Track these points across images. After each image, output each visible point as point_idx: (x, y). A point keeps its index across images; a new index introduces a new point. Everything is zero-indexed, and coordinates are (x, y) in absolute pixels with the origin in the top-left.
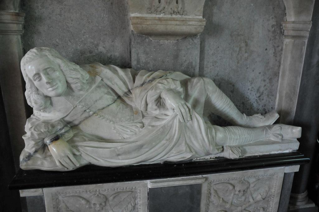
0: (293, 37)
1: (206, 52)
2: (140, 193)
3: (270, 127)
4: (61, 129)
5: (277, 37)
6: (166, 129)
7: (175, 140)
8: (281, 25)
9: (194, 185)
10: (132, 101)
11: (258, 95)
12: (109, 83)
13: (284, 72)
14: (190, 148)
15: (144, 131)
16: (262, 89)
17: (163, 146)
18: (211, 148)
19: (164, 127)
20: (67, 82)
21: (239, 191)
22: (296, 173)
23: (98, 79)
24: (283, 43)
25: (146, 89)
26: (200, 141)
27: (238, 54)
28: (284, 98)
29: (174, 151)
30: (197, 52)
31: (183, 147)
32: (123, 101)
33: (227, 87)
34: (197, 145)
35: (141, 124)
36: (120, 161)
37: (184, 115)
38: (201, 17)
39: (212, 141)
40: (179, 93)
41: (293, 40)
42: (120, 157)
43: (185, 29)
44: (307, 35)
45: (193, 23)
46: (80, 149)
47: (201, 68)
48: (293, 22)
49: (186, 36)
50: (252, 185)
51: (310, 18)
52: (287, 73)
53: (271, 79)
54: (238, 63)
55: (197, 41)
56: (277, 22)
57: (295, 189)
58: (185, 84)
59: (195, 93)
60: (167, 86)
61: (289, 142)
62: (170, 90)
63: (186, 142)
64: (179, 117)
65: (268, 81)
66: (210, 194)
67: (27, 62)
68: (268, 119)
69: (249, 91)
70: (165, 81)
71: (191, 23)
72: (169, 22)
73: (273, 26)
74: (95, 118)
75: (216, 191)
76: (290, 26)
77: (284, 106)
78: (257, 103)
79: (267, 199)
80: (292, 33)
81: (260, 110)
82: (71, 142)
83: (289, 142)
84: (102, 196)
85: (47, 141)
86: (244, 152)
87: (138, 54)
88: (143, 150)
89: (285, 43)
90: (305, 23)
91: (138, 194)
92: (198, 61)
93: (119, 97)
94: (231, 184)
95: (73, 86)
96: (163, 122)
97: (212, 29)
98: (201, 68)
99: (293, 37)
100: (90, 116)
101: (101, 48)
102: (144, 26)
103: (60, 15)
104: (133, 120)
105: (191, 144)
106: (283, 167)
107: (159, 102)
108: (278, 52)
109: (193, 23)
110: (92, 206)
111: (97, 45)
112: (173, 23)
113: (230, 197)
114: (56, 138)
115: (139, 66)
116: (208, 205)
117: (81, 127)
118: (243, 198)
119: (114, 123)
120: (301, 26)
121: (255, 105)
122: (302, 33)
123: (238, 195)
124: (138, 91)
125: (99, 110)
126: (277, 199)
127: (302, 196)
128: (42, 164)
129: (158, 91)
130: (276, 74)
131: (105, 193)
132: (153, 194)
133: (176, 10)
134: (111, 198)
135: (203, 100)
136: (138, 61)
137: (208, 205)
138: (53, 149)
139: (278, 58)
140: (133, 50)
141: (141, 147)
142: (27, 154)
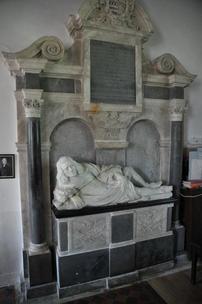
0: (165, 147)
1: (127, 156)
2: (108, 219)
3: (159, 187)
4: (75, 191)
5: (158, 147)
6: (118, 188)
7: (122, 193)
8: (159, 142)
9: (131, 214)
10: (101, 178)
11: (151, 174)
12: (91, 171)
13: (162, 163)
14: (128, 196)
15: (109, 190)
16: (153, 171)
17: (117, 196)
18: (137, 196)
19: (117, 188)
20: (77, 171)
21: (149, 217)
22: (172, 207)
23: (87, 169)
24: (160, 150)
25: (108, 173)
26: (131, 194)
27: (141, 156)
28: (163, 175)
29: (122, 198)
30: (124, 156)
31: (126, 196)
32: (97, 179)
33: (139, 171)
34: (131, 195)
35: (106, 188)
36: (101, 203)
37: (125, 182)
38: (126, 141)
39: (137, 192)
40: (121, 173)
41: (164, 148)
42: (101, 201)
43: (120, 146)
44: (170, 146)
45: (124, 144)
46: (84, 199)
47: (126, 163)
48: (164, 141)
49: (119, 149)
50: (154, 214)
51: (171, 139)
52: (164, 163)
53: (156, 167)
54: (141, 160)
55: (124, 151)
56: (157, 140)
57: (173, 220)
58: (122, 170)
59: (127, 173)
60: (116, 171)
61: (168, 193)
62: (118, 172)
63: (127, 194)
64: (123, 183)
65: (155, 167)
66: (137, 219)
67: (63, 163)
68: (158, 184)
69: (147, 173)
70: (115, 169)
71: (123, 144)
72: (114, 144)
73: (155, 142)
74: (88, 186)
75: (139, 218)
76: (163, 142)
77: (164, 178)
78: (151, 178)
79: (161, 221)
80: (164, 145)
81: (177, 107)
82: (79, 196)
83: (168, 193)
84: (92, 222)
85: (70, 196)
86: (150, 198)
87: (99, 158)
88: (110, 198)
89: (161, 149)
90: (168, 141)
91: (107, 220)
92: (125, 160)
93: (95, 177)
94: (146, 214)
95: (79, 172)
96: (116, 186)
97: (131, 145)
98: (126, 163)
99: (165, 147)
100: (86, 185)
101: (82, 156)
102: (104, 146)
103: (66, 142)
104: (103, 186)
105: (128, 195)
106: (167, 205)
107: (114, 178)
108: (158, 154)
109: (124, 144)
110: (87, 226)
111: (81, 155)
112: (116, 144)
113: (145, 220)
114: (74, 195)
115: (99, 163)
116: (136, 225)
117: (82, 190)
118: (151, 220)
119: (95, 188)
120: (167, 142)
121: (150, 179)
122: (168, 145)
123: (149, 219)
124: (104, 174)
125: (89, 182)
126: (166, 221)
127: (177, 222)
128: (69, 206)
129: (113, 173)
130: (159, 164)
131: (93, 220)
132: (114, 219)
133: (116, 138)
134: (95, 223)
135: (130, 176)
136: (99, 161)
137: (136, 225)
138: (73, 199)
139: (159, 157)
140: (97, 156)
141: (109, 196)
142: (62, 203)
